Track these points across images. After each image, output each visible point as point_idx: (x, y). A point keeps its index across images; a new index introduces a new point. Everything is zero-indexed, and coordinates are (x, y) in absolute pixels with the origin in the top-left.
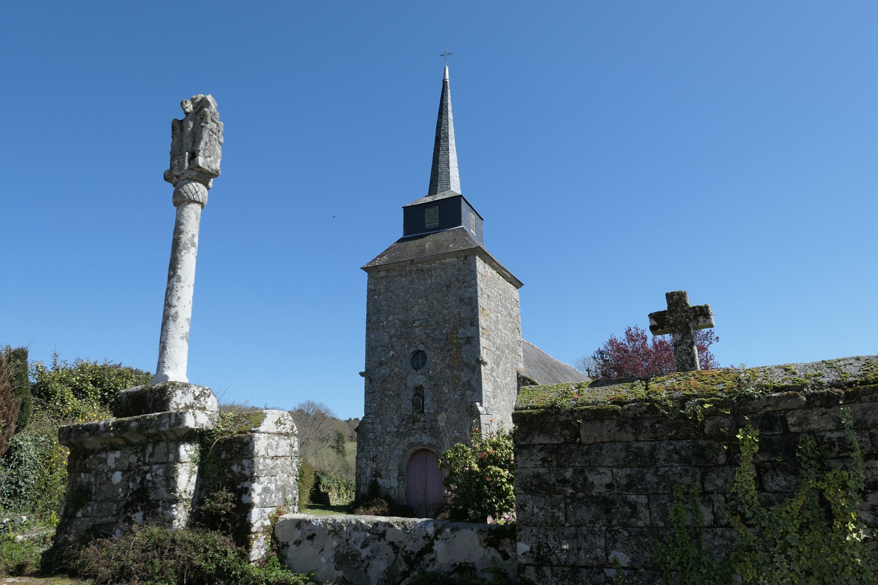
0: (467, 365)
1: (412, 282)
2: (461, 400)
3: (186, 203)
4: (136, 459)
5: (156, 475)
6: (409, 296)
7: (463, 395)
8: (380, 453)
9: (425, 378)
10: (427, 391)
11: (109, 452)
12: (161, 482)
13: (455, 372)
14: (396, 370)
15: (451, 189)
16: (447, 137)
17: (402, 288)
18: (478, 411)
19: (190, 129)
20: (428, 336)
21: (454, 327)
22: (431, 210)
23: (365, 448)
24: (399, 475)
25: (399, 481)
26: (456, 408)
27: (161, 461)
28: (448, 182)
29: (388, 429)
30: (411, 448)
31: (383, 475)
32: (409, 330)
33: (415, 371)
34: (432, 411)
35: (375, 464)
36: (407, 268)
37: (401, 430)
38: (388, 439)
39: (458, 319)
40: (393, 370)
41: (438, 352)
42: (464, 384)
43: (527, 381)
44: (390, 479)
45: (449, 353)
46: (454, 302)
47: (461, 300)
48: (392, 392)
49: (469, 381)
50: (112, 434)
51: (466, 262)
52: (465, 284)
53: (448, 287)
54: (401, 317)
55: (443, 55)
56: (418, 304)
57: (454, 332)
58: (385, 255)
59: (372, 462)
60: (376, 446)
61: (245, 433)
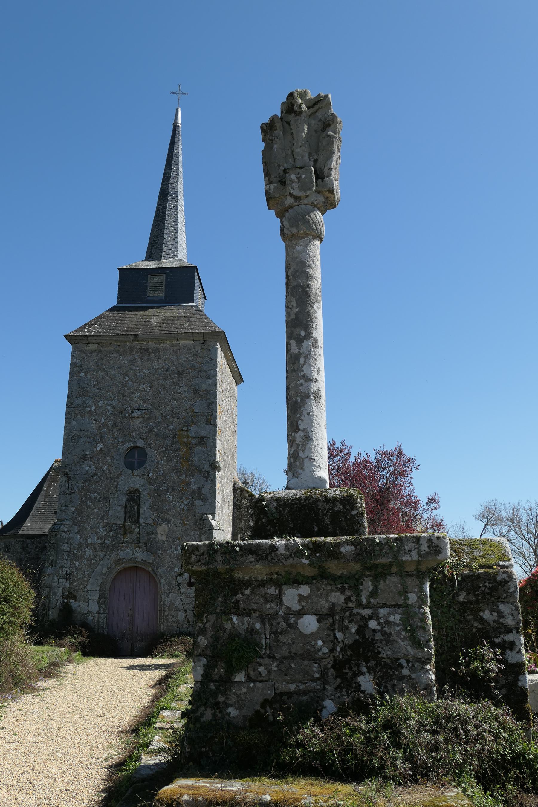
0: (199, 470)
1: (133, 362)
2: (189, 510)
3: (311, 237)
4: (342, 598)
5: (388, 623)
6: (127, 379)
7: (191, 505)
8: (77, 569)
9: (142, 481)
10: (144, 496)
11: (283, 586)
12: (399, 633)
13: (183, 476)
14: (105, 468)
15: (179, 258)
16: (177, 194)
17: (119, 368)
18: (211, 525)
19: (304, 135)
20: (151, 430)
21: (185, 422)
22: (156, 278)
23: (58, 562)
24: (101, 597)
25: (99, 604)
26: (181, 520)
27: (393, 603)
28: (175, 249)
29: (90, 540)
30: (118, 565)
31: (78, 596)
32: (125, 420)
33: (130, 471)
34: (150, 521)
35: (68, 582)
36: (128, 344)
37: (107, 542)
38: (89, 552)
39: (190, 414)
40: (101, 468)
41: (163, 451)
42: (193, 492)
43: (244, 492)
44: (88, 602)
45: (177, 454)
46: (186, 393)
47: (196, 392)
48: (98, 494)
49: (199, 489)
50: (306, 562)
51: (204, 347)
52: (202, 374)
53: (179, 374)
54: (115, 403)
55: (183, 94)
56: (140, 391)
57: (185, 429)
58: (95, 323)
59: (64, 580)
60: (71, 561)
61: (491, 567)
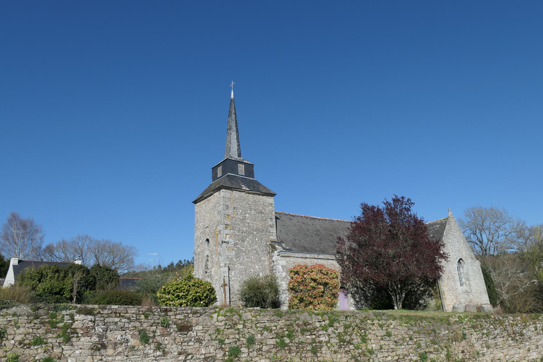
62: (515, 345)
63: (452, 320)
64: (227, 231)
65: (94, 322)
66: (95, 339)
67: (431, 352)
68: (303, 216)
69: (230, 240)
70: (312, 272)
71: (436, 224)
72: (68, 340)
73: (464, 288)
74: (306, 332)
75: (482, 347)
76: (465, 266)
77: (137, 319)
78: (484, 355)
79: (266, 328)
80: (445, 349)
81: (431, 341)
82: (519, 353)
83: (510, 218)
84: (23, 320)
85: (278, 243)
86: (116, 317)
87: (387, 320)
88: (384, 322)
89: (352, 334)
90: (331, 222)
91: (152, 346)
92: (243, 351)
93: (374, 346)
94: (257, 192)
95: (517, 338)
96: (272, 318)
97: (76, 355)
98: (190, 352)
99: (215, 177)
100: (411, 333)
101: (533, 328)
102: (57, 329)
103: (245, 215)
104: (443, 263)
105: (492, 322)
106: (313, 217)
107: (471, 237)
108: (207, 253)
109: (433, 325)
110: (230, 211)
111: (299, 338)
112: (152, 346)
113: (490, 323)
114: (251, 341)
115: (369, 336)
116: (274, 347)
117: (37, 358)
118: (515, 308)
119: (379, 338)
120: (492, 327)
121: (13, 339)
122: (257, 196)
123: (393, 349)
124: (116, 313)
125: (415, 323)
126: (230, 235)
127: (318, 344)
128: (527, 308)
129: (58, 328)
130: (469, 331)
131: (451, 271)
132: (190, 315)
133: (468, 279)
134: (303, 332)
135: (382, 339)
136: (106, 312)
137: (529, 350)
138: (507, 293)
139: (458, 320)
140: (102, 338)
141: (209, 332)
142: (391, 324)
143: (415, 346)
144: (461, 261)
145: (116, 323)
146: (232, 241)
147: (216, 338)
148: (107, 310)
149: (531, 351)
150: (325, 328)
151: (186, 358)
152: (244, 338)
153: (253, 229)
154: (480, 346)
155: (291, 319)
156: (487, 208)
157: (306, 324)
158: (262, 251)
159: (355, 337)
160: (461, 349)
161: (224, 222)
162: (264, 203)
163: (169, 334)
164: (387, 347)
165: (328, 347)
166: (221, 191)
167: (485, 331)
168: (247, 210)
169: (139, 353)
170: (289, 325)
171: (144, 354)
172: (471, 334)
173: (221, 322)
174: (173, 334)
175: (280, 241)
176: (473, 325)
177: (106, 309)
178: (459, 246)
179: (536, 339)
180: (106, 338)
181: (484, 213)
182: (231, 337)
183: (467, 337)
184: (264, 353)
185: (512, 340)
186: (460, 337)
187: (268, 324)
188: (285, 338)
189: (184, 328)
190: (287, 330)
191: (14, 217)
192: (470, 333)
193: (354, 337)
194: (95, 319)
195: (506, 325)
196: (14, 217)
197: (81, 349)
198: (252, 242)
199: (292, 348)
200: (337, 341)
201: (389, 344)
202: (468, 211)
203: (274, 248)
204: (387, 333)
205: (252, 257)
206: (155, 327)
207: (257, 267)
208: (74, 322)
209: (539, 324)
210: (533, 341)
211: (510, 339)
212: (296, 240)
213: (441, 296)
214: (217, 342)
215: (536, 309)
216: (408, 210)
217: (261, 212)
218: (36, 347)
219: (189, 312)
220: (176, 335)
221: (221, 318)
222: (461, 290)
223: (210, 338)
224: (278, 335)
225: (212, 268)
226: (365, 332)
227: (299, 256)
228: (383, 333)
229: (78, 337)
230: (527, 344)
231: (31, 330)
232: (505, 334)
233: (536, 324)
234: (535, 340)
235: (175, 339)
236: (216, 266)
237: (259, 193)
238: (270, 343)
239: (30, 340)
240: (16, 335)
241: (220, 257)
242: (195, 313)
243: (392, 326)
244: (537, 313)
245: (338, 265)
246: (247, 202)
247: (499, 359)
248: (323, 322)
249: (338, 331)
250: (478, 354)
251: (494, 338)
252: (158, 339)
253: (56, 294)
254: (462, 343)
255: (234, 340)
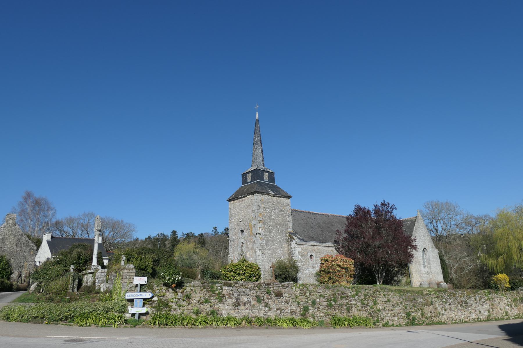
22: (138, 301)
53: (249, 206)
54: (237, 218)
62: (462, 310)
63: (425, 292)
64: (259, 226)
65: (233, 291)
66: (234, 300)
67: (412, 312)
68: (307, 211)
69: (262, 232)
70: (337, 260)
71: (407, 221)
72: (221, 301)
73: (426, 269)
74: (343, 298)
75: (442, 310)
76: (427, 254)
77: (254, 290)
78: (443, 315)
79: (321, 296)
80: (421, 310)
81: (413, 305)
82: (464, 315)
83: (461, 211)
84: (198, 289)
85: (294, 234)
86: (243, 288)
87: (388, 292)
88: (386, 293)
89: (368, 300)
90: (327, 216)
91: (263, 305)
92: (310, 309)
93: (380, 307)
94: (279, 196)
95: (464, 305)
96: (325, 290)
97: (226, 309)
98: (283, 308)
99: (244, 181)
100: (401, 300)
101: (474, 299)
102: (215, 294)
103: (271, 213)
104: (413, 252)
105: (448, 294)
106: (314, 212)
107: (429, 225)
108: (242, 240)
109: (414, 296)
110: (261, 211)
111: (340, 302)
112: (263, 305)
113: (447, 295)
114: (314, 303)
115: (378, 301)
116: (326, 307)
117: (207, 310)
118: (461, 284)
119: (384, 303)
120: (448, 297)
121: (195, 300)
122: (279, 198)
123: (391, 309)
124: (243, 286)
125: (404, 294)
126: (262, 228)
127: (350, 305)
128: (470, 285)
129: (216, 294)
130: (435, 300)
131: (418, 257)
132: (281, 288)
133: (429, 264)
134: (342, 298)
135: (385, 303)
136: (238, 285)
137: (470, 313)
138: (455, 273)
139: (428, 292)
140: (238, 300)
141: (292, 297)
142: (390, 294)
143: (404, 308)
144: (425, 250)
145: (244, 292)
146: (263, 233)
147: (295, 301)
148: (238, 284)
149: (472, 314)
150: (353, 296)
151: (281, 312)
152: (310, 301)
153: (276, 224)
154: (441, 309)
155: (334, 290)
156: (443, 202)
157: (343, 293)
158: (283, 240)
159: (370, 302)
160: (430, 310)
161: (258, 219)
162: (284, 203)
163: (271, 298)
164: (388, 308)
165: (356, 307)
166: (255, 195)
167: (444, 300)
168: (273, 209)
169: (257, 308)
170: (333, 294)
171: (259, 309)
172: (436, 302)
173: (298, 291)
174: (273, 298)
175: (295, 232)
176: (437, 296)
177: (237, 283)
178: (424, 239)
179: (475, 306)
180: (240, 300)
181: (440, 207)
182: (304, 300)
183: (434, 303)
184: (321, 310)
185: (460, 306)
186: (429, 304)
187: (322, 293)
188: (332, 302)
189: (279, 295)
190: (333, 297)
191: (28, 195)
192: (435, 301)
193: (369, 301)
194: (233, 289)
195: (457, 297)
196: (28, 195)
197: (228, 306)
198: (277, 233)
199: (336, 307)
200: (361, 304)
201: (389, 306)
202: (428, 204)
203: (292, 239)
204: (388, 299)
205: (277, 244)
206: (264, 294)
207: (280, 252)
208: (223, 291)
209: (478, 296)
210: (473, 307)
211: (459, 305)
212: (305, 231)
213: (410, 276)
214: (296, 303)
215: (477, 286)
216: (391, 212)
217: (282, 211)
218: (206, 304)
219: (280, 285)
220: (275, 299)
221: (297, 289)
222: (424, 271)
223: (292, 301)
224: (328, 300)
225: (247, 252)
226: (376, 299)
227: (310, 244)
228: (386, 300)
229: (226, 299)
230: (469, 309)
231: (203, 295)
232: (456, 302)
233: (476, 296)
234: (475, 307)
235: (274, 301)
236: (250, 251)
237: (281, 196)
238: (324, 304)
239: (203, 300)
240: (196, 298)
241: (254, 244)
242: (283, 286)
243: (391, 296)
244: (477, 289)
245: (335, 251)
246: (273, 203)
247: (452, 318)
248: (353, 293)
249: (361, 298)
250: (439, 314)
251: (449, 305)
252: (267, 301)
253: (142, 270)
254: (431, 307)
255: (305, 302)
